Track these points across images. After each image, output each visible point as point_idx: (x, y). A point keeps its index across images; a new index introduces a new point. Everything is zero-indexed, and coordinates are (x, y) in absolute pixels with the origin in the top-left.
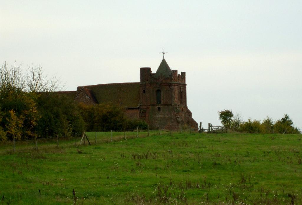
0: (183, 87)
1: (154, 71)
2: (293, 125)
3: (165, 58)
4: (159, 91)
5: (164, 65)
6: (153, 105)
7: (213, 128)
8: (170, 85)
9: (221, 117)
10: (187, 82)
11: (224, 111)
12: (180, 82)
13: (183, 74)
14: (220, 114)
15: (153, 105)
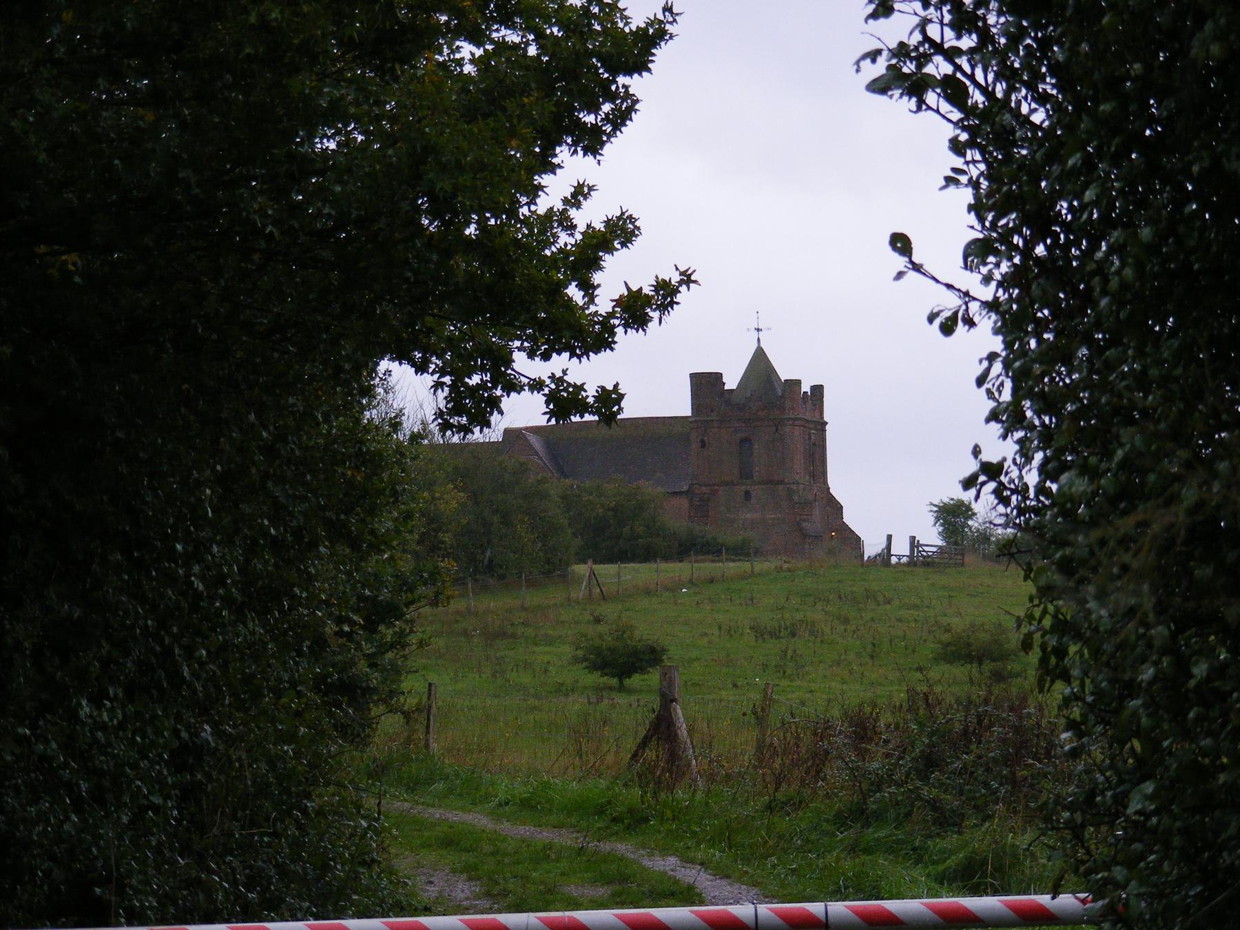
0: (816, 430)
1: (731, 382)
2: (973, 202)
3: (762, 345)
4: (745, 441)
5: (760, 363)
6: (730, 484)
7: (924, 551)
8: (778, 424)
9: (937, 519)
10: (830, 413)
11: (946, 500)
12: (808, 416)
13: (818, 390)
14: (935, 509)
15: (730, 484)
